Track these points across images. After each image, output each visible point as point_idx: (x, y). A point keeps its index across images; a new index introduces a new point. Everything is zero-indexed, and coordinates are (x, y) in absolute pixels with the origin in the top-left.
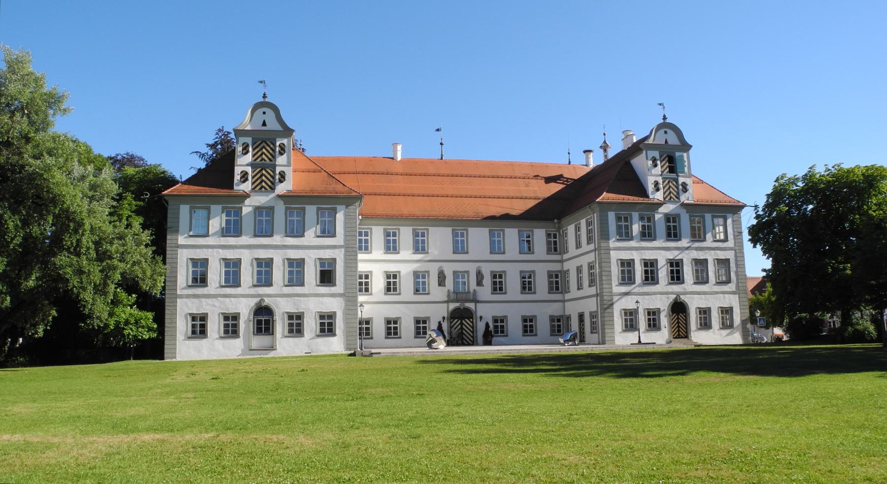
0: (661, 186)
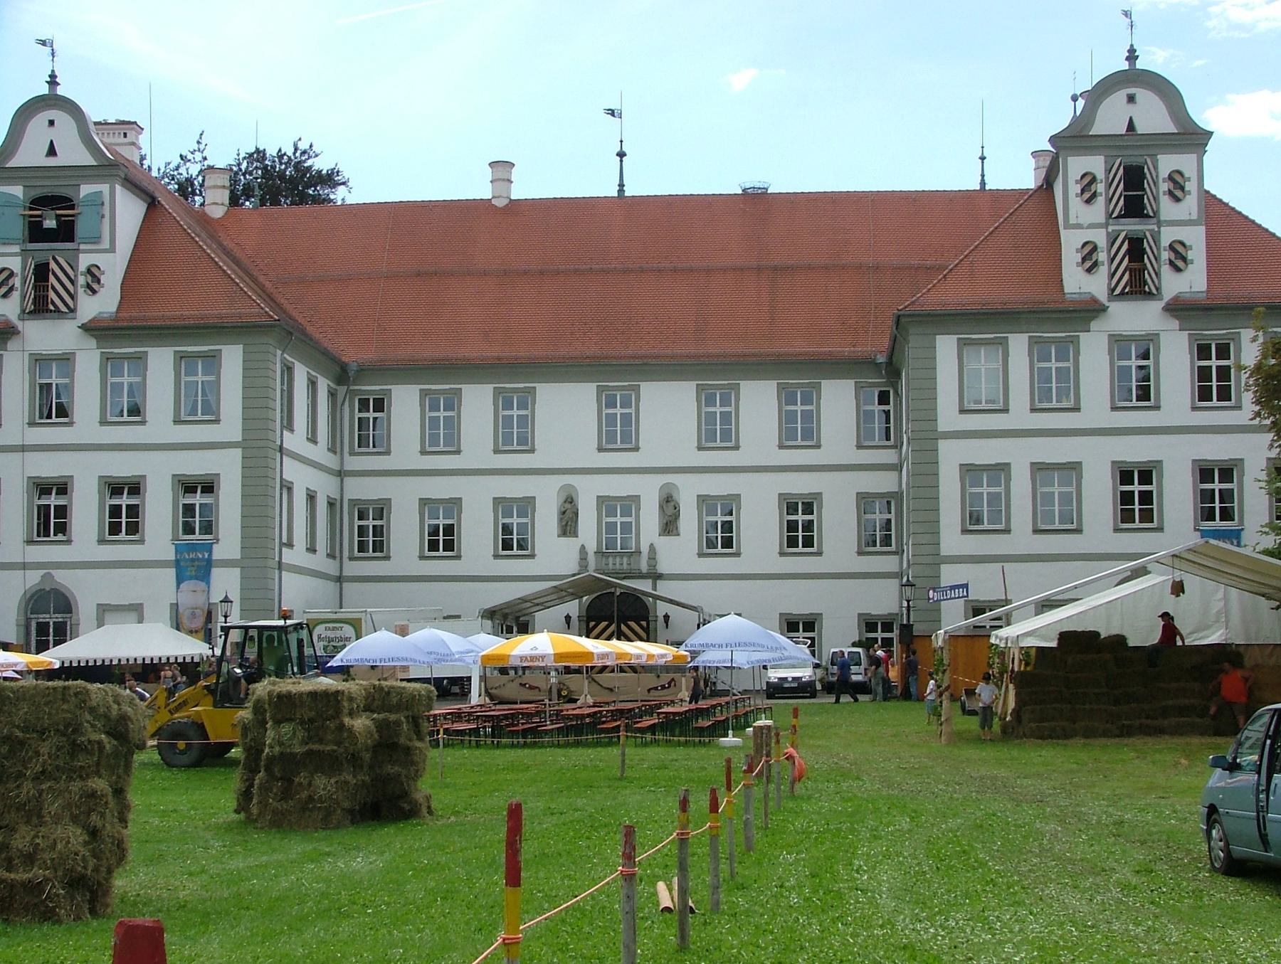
0: (1102, 256)
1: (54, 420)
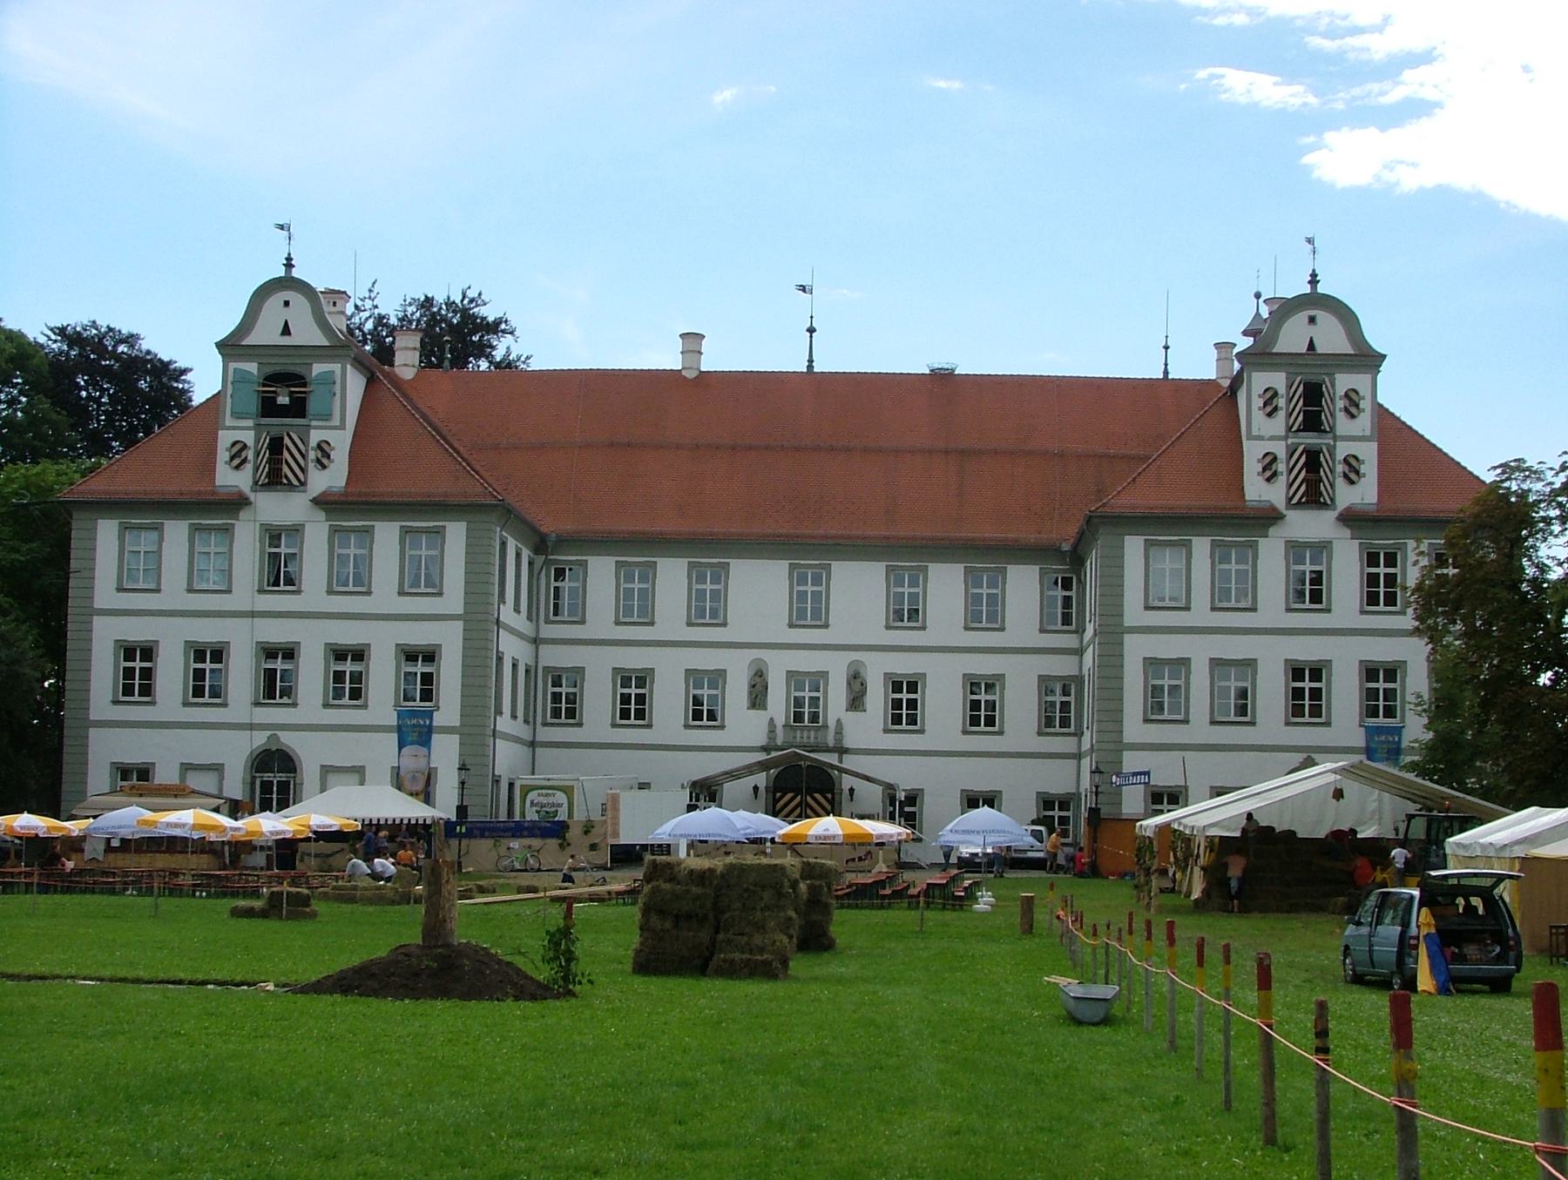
0: (1281, 467)
1: (282, 588)
